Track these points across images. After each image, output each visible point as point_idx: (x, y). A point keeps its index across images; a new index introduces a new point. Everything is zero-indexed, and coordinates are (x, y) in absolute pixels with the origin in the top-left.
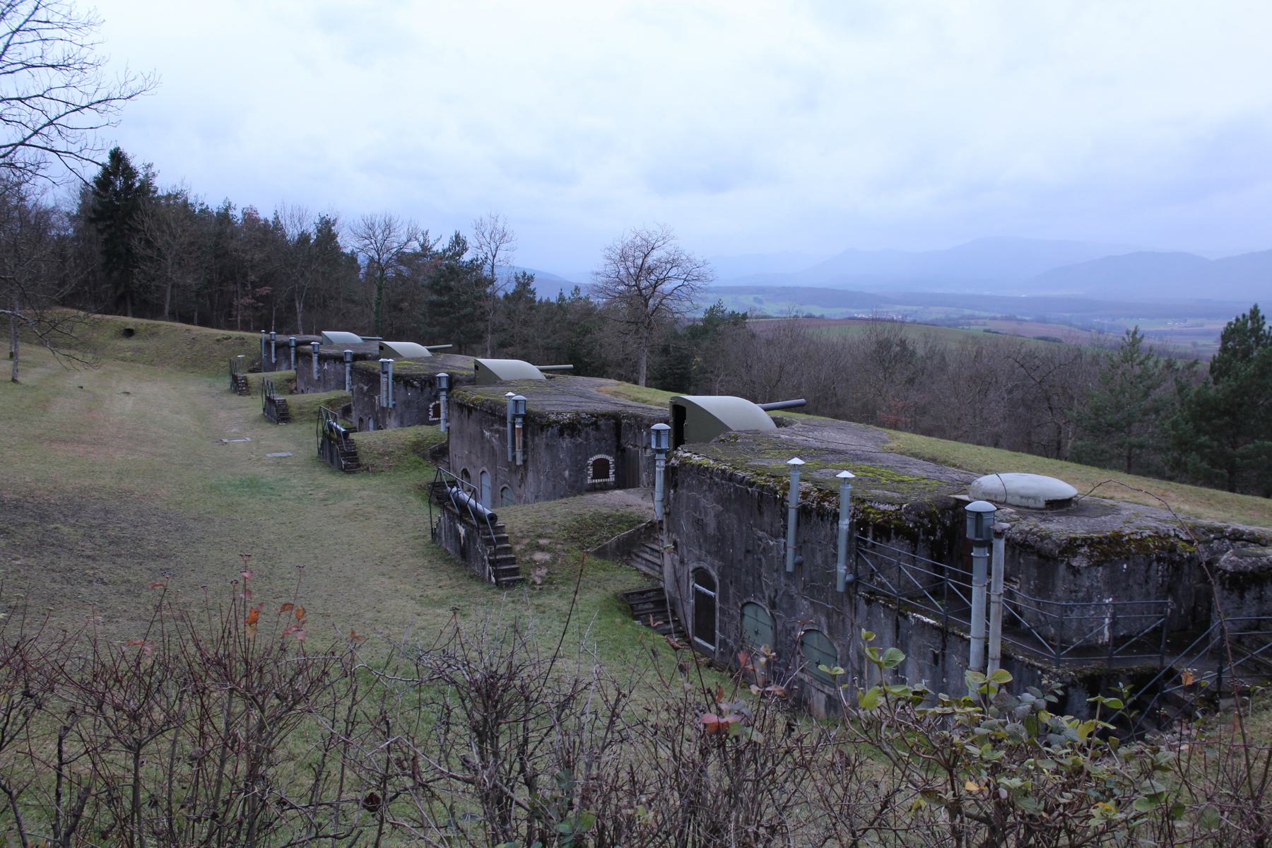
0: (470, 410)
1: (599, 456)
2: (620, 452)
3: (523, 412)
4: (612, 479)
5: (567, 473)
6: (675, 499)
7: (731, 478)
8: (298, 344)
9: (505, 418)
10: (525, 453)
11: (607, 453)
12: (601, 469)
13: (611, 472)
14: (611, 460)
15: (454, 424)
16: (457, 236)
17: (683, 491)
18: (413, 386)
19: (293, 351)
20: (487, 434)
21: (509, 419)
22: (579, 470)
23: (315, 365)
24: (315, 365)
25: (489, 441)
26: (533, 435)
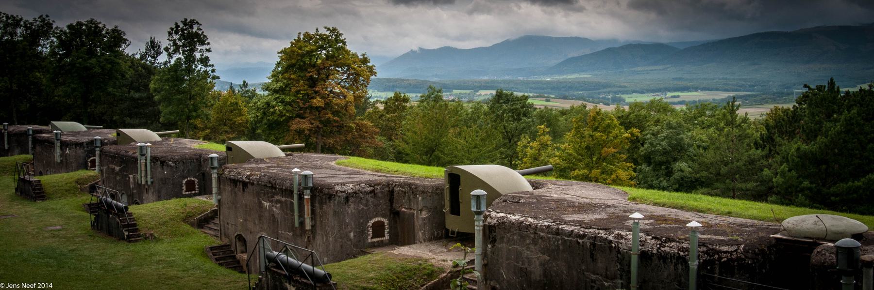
0: (245, 184)
1: (376, 219)
2: (395, 215)
3: (311, 185)
4: (387, 237)
5: (352, 234)
6: (493, 253)
7: (558, 232)
8: (36, 132)
9: (292, 192)
10: (313, 219)
11: (384, 216)
12: (378, 229)
13: (386, 231)
14: (386, 221)
15: (226, 196)
16: (152, 42)
17: (498, 245)
18: (168, 166)
19: (30, 138)
20: (266, 204)
21: (295, 191)
22: (362, 233)
23: (58, 151)
24: (58, 151)
25: (270, 210)
26: (321, 204)
